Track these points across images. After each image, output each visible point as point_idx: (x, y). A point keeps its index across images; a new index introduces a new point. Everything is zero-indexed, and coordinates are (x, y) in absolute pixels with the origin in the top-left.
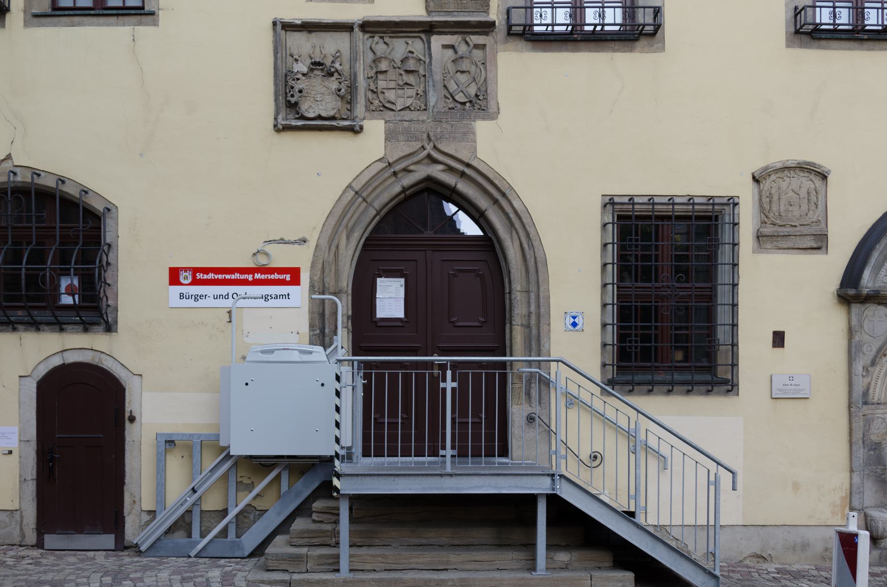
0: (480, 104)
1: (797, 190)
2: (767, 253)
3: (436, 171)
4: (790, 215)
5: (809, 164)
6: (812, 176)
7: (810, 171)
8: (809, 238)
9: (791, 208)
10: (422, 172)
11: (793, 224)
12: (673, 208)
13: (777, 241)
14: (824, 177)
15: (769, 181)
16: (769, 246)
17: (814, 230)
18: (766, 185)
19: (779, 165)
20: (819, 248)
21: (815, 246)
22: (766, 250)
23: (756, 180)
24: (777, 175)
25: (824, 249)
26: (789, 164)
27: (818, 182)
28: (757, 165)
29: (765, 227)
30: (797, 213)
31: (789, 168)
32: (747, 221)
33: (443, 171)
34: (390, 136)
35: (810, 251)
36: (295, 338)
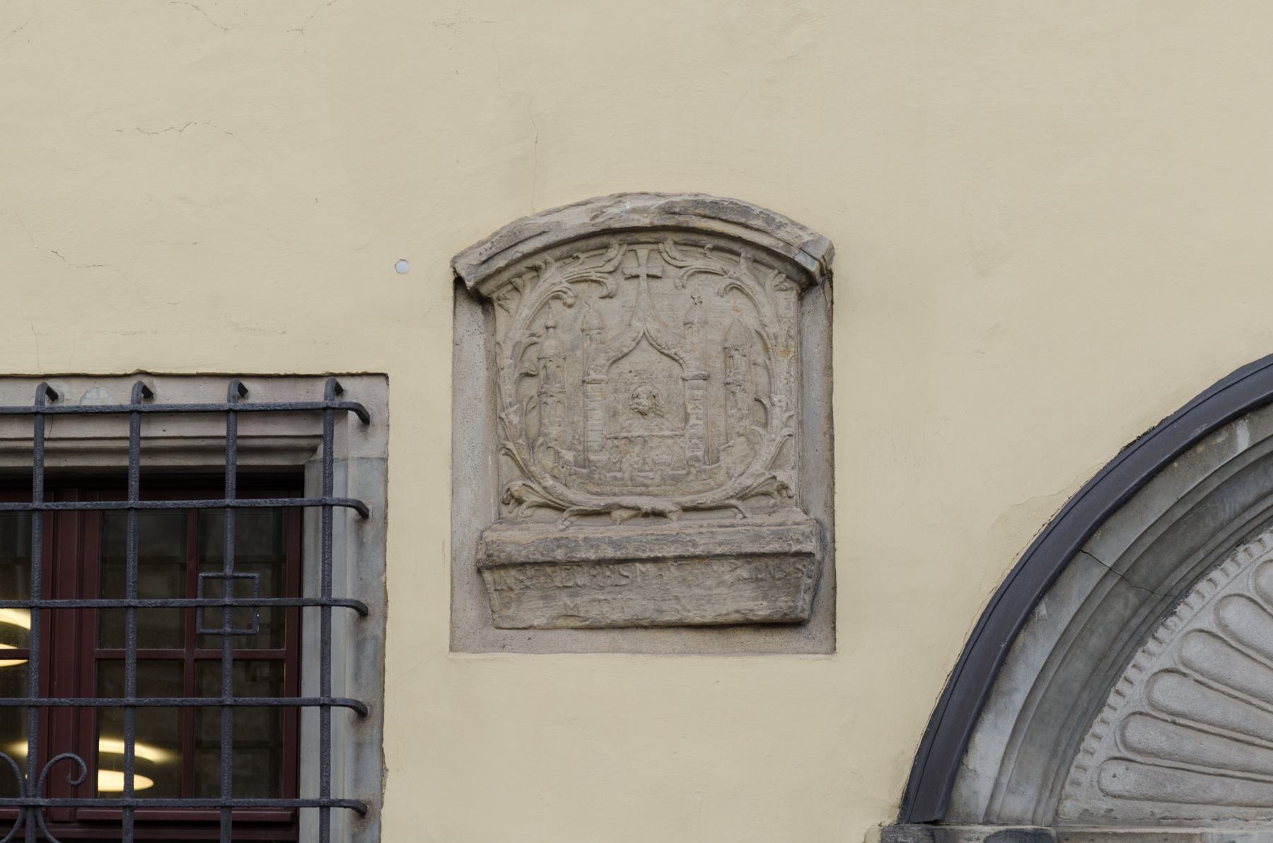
1: (666, 339)
2: (531, 649)
4: (634, 456)
5: (715, 209)
6: (741, 270)
7: (728, 245)
8: (723, 570)
9: (638, 428)
11: (646, 503)
12: (39, 437)
13: (574, 590)
14: (812, 282)
15: (532, 295)
16: (534, 611)
17: (757, 528)
18: (517, 313)
19: (577, 222)
20: (789, 624)
21: (762, 610)
22: (524, 635)
23: (474, 294)
24: (574, 270)
25: (817, 627)
26: (619, 216)
27: (774, 301)
28: (479, 219)
29: (513, 523)
30: (663, 453)
31: (629, 234)
32: (420, 504)
33: (533, 289)
35: (746, 637)
36: (821, 299)
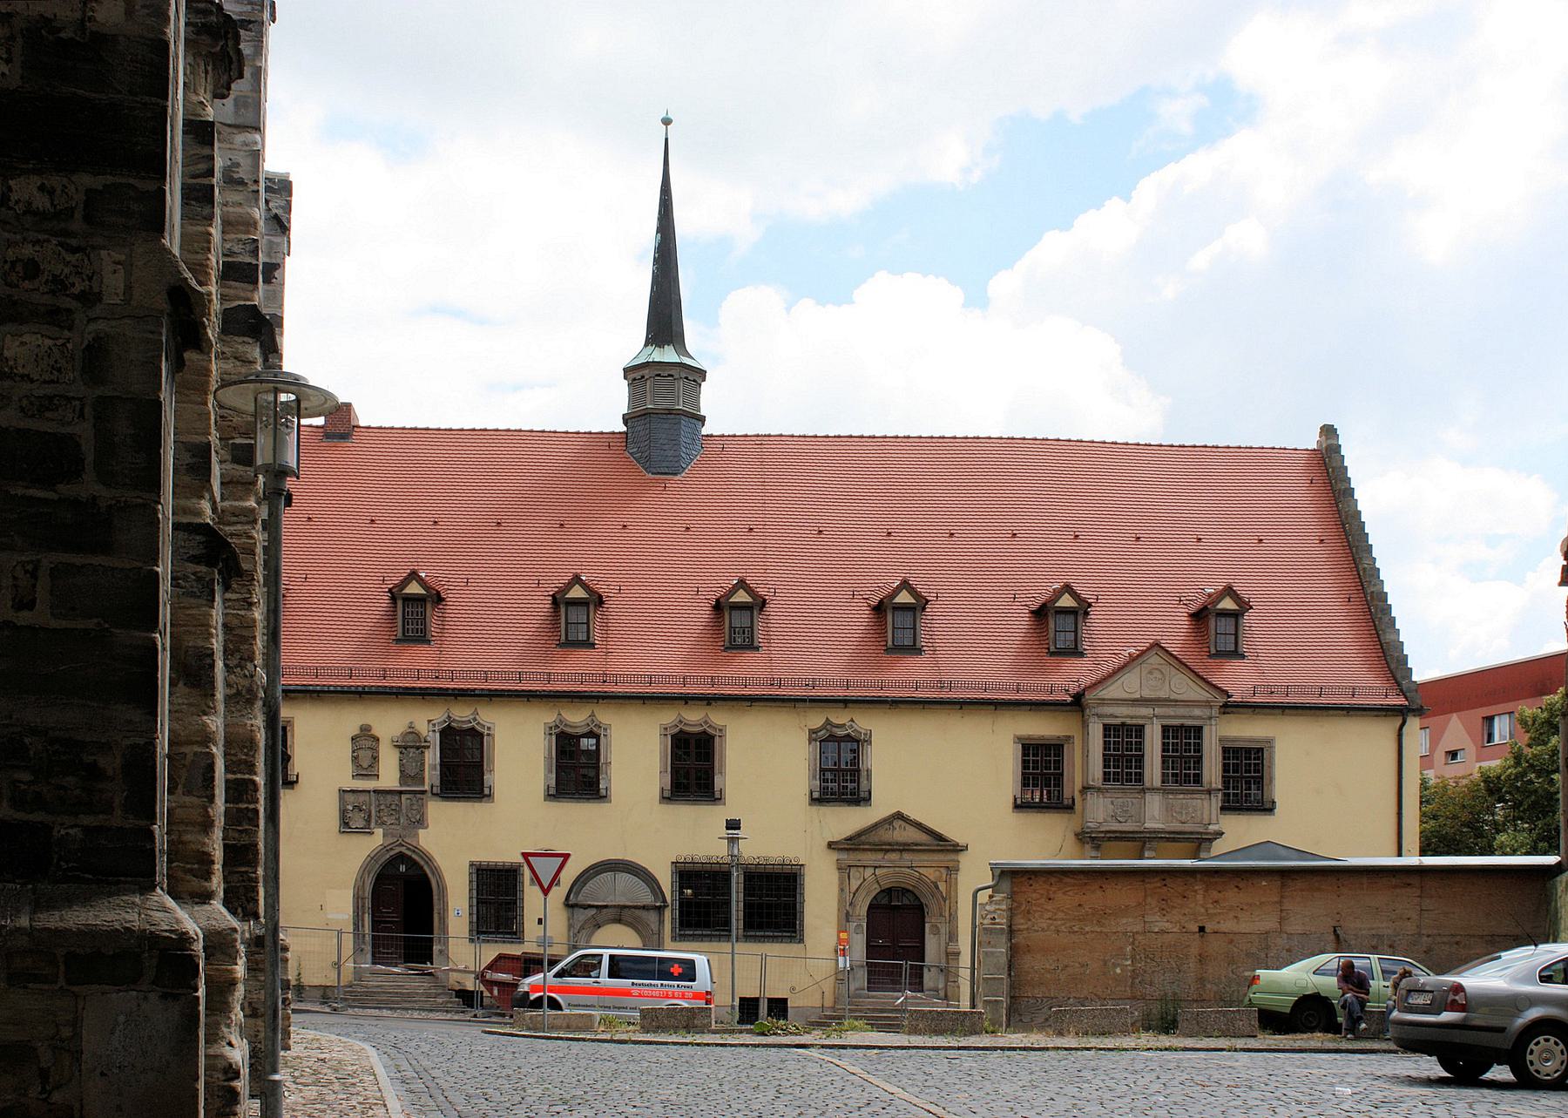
0: (421, 822)
3: (403, 849)
10: (397, 850)
34: (384, 835)
